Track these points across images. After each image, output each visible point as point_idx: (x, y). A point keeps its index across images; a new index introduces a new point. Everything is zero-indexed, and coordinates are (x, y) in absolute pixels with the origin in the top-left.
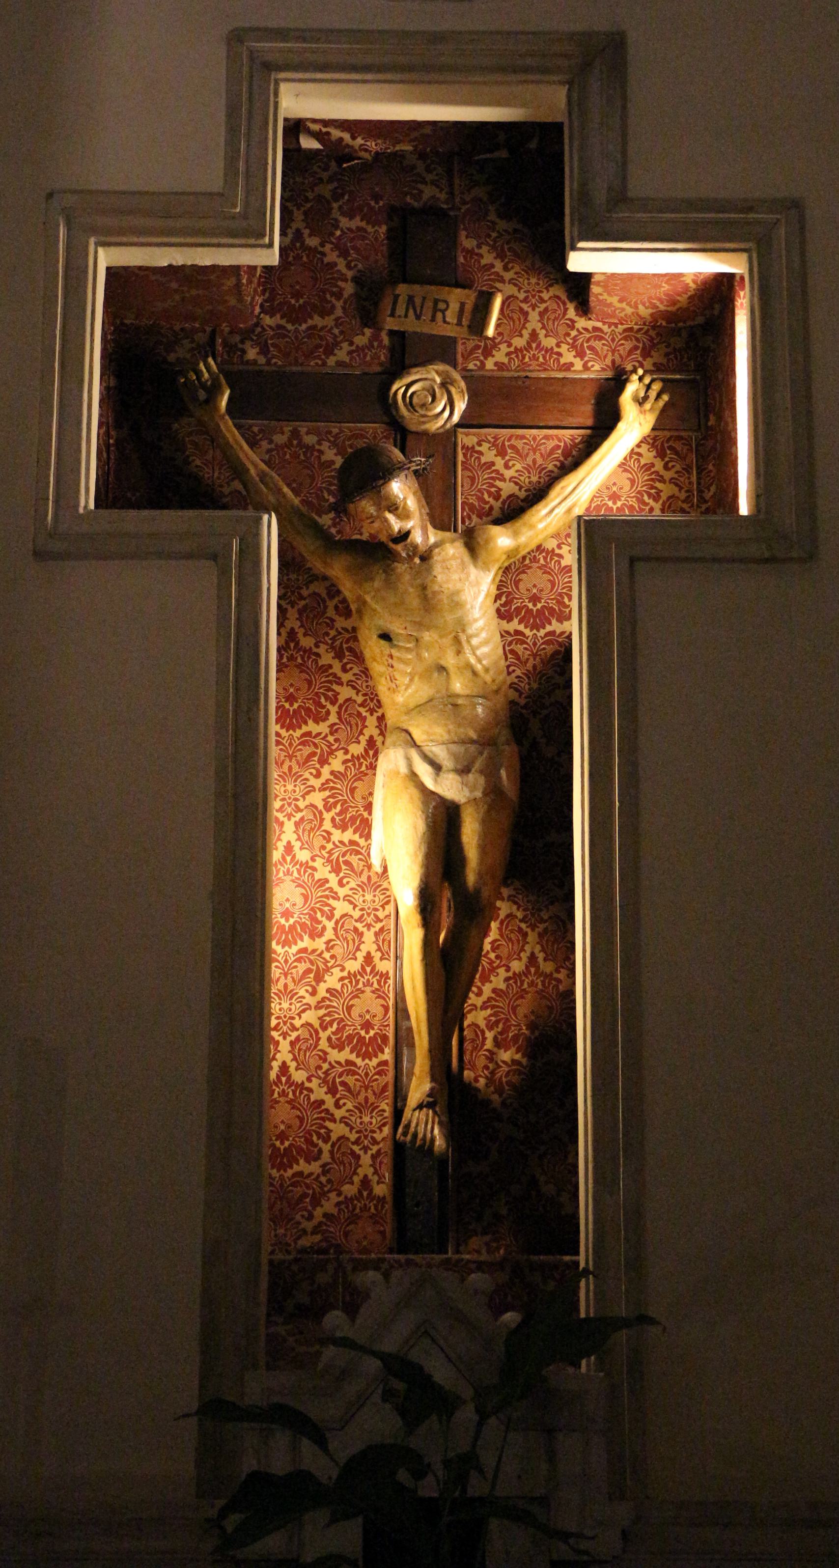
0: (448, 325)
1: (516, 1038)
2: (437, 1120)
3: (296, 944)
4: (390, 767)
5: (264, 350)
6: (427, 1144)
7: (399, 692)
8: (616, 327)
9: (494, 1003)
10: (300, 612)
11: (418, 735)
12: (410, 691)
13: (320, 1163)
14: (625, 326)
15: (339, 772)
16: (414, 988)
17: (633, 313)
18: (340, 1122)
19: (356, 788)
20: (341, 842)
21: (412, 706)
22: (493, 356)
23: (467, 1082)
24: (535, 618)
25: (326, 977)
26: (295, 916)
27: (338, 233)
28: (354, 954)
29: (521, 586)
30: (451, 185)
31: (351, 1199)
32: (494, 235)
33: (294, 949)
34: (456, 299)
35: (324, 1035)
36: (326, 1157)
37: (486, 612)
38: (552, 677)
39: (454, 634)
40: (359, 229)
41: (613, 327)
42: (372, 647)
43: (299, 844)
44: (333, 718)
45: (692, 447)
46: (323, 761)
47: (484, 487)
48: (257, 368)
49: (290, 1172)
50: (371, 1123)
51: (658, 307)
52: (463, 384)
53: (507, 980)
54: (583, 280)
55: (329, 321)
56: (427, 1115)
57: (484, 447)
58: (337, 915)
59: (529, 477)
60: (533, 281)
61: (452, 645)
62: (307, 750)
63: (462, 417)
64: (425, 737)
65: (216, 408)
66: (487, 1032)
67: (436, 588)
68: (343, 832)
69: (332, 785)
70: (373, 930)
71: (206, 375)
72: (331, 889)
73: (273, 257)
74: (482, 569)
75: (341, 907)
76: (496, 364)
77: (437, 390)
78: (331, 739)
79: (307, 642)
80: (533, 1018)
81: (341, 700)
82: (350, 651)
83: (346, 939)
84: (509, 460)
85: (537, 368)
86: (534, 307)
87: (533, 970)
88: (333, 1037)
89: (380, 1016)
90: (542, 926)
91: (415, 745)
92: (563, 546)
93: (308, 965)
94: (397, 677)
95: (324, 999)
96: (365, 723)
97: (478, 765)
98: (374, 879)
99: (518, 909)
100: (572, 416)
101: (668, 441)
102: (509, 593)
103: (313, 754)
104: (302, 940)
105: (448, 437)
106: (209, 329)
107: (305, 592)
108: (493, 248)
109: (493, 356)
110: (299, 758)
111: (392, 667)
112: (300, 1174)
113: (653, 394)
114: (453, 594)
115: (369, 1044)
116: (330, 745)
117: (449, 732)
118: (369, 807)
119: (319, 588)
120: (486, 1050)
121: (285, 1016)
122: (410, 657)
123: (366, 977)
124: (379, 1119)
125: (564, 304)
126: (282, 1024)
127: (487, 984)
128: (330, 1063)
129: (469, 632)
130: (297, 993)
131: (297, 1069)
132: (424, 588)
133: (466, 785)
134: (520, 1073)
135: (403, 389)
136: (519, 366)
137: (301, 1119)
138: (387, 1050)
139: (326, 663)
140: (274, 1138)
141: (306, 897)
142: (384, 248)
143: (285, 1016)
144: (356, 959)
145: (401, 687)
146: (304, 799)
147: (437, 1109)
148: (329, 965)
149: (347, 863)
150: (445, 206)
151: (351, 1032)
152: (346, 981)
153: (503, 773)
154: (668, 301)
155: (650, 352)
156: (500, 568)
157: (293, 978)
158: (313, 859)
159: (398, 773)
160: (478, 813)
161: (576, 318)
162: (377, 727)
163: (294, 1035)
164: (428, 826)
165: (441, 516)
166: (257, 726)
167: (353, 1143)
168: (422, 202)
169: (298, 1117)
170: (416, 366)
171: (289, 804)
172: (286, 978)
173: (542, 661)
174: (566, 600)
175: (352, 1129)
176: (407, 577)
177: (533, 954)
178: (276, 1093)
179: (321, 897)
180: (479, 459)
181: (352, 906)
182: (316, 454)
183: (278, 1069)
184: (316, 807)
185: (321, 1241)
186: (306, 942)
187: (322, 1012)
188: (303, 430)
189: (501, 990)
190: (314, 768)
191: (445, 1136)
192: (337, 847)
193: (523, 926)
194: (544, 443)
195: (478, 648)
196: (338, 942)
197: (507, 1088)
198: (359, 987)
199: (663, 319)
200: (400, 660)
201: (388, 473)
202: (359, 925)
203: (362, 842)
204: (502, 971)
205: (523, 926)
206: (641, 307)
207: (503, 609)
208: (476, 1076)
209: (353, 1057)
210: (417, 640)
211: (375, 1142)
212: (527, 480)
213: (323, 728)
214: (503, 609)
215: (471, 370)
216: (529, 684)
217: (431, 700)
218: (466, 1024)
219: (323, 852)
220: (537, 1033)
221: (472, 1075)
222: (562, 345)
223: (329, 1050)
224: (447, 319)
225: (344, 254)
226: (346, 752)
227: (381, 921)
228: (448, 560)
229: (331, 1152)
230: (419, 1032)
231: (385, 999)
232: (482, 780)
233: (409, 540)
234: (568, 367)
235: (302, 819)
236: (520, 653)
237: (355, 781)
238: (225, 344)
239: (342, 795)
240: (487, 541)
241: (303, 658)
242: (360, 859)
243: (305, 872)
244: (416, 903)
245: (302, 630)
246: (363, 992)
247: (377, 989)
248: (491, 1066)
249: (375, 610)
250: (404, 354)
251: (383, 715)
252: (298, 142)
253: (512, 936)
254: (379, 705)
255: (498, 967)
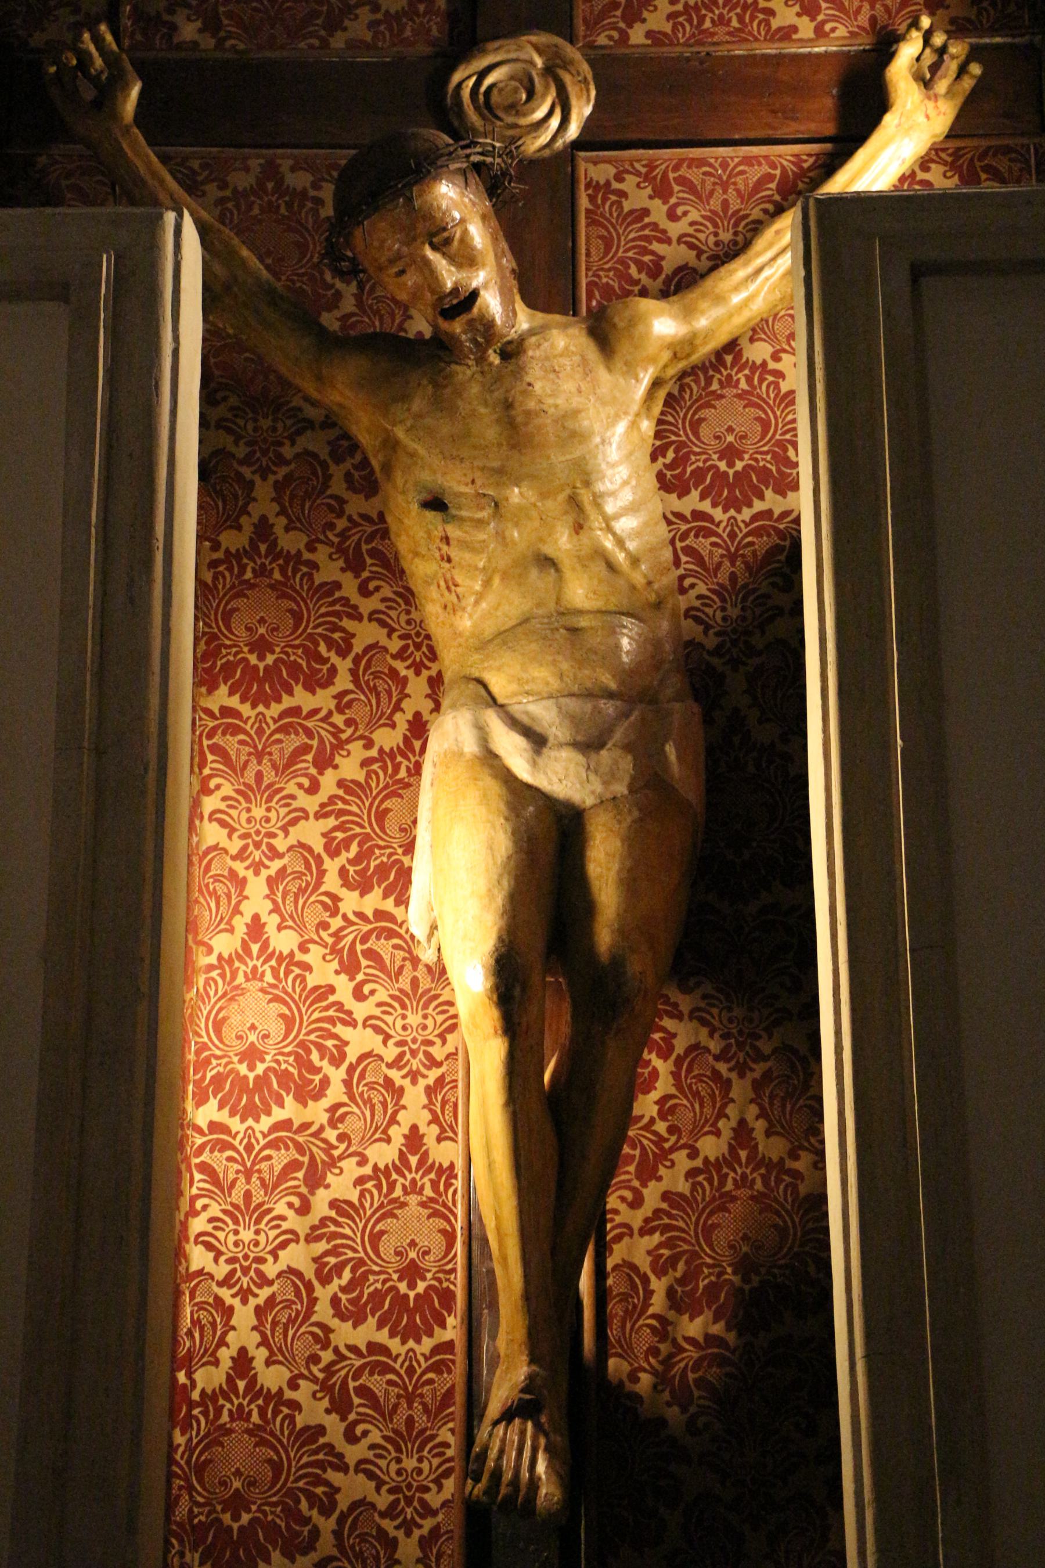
1: (712, 1290)
2: (542, 1441)
3: (269, 1113)
5: (212, 25)
11: (499, 685)
15: (353, 781)
16: (490, 1166)
19: (387, 811)
20: (360, 915)
21: (488, 633)
22: (644, 21)
23: (615, 1381)
24: (731, 488)
25: (330, 1178)
29: (704, 431)
33: (266, 1123)
35: (324, 1294)
37: (631, 454)
38: (767, 596)
39: (568, 491)
42: (413, 530)
43: (275, 919)
44: (343, 682)
46: (324, 762)
47: (630, 254)
50: (420, 1471)
52: (585, 68)
56: (523, 1433)
57: (629, 183)
59: (716, 234)
61: (566, 513)
63: (588, 126)
64: (514, 687)
65: (115, 116)
66: (653, 1278)
67: (532, 405)
68: (362, 895)
70: (422, 1083)
71: (99, 62)
72: (339, 1006)
75: (359, 1041)
76: (649, 34)
77: (537, 80)
78: (338, 719)
79: (291, 541)
81: (358, 648)
82: (376, 556)
87: (743, 1154)
88: (344, 1297)
89: (437, 1252)
90: (759, 1069)
91: (493, 701)
94: (459, 579)
95: (324, 1221)
96: (404, 675)
97: (618, 735)
99: (711, 1035)
100: (795, 119)
101: (983, 156)
102: (681, 445)
103: (305, 749)
104: (281, 1105)
105: (560, 165)
107: (288, 452)
109: (644, 21)
110: (275, 757)
111: (449, 560)
116: (337, 732)
118: (409, 848)
119: (315, 442)
120: (653, 1316)
124: (436, 1462)
126: (239, 1273)
128: (336, 1350)
129: (600, 487)
131: (268, 1363)
132: (508, 406)
134: (722, 1361)
135: (474, 79)
136: (693, 35)
137: (277, 1468)
138: (451, 1321)
141: (289, 1022)
144: (388, 1140)
145: (466, 599)
147: (543, 1419)
148: (336, 1153)
149: (370, 954)
152: (369, 1185)
153: (671, 751)
158: (303, 948)
159: (461, 754)
160: (620, 822)
162: (428, 696)
163: (265, 1293)
164: (516, 843)
165: (547, 278)
169: (270, 1461)
170: (496, 38)
171: (257, 845)
173: (748, 567)
176: (475, 389)
178: (225, 1412)
179: (318, 1020)
180: (619, 204)
182: (309, 205)
184: (310, 850)
186: (289, 1110)
187: (322, 1246)
188: (285, 165)
189: (681, 1195)
190: (306, 775)
191: (560, 1477)
193: (722, 1067)
195: (617, 517)
196: (355, 1109)
200: (465, 545)
201: (424, 168)
202: (395, 1075)
203: (398, 912)
204: (681, 1157)
205: (722, 1067)
207: (669, 473)
208: (631, 1369)
209: (382, 1337)
210: (496, 505)
211: (428, 1511)
212: (712, 240)
213: (323, 699)
214: (669, 473)
216: (723, 609)
217: (526, 620)
218: (610, 1263)
219: (324, 934)
220: (756, 1280)
221: (626, 1367)
223: (334, 1323)
226: (369, 744)
227: (439, 1065)
228: (555, 357)
229: (337, 1534)
230: (504, 1259)
231: (449, 1221)
232: (627, 764)
233: (475, 310)
234: (788, 33)
237: (386, 797)
240: (632, 323)
243: (287, 973)
244: (489, 985)
245: (283, 521)
249: (413, 455)
251: (440, 674)
255: (673, 1149)
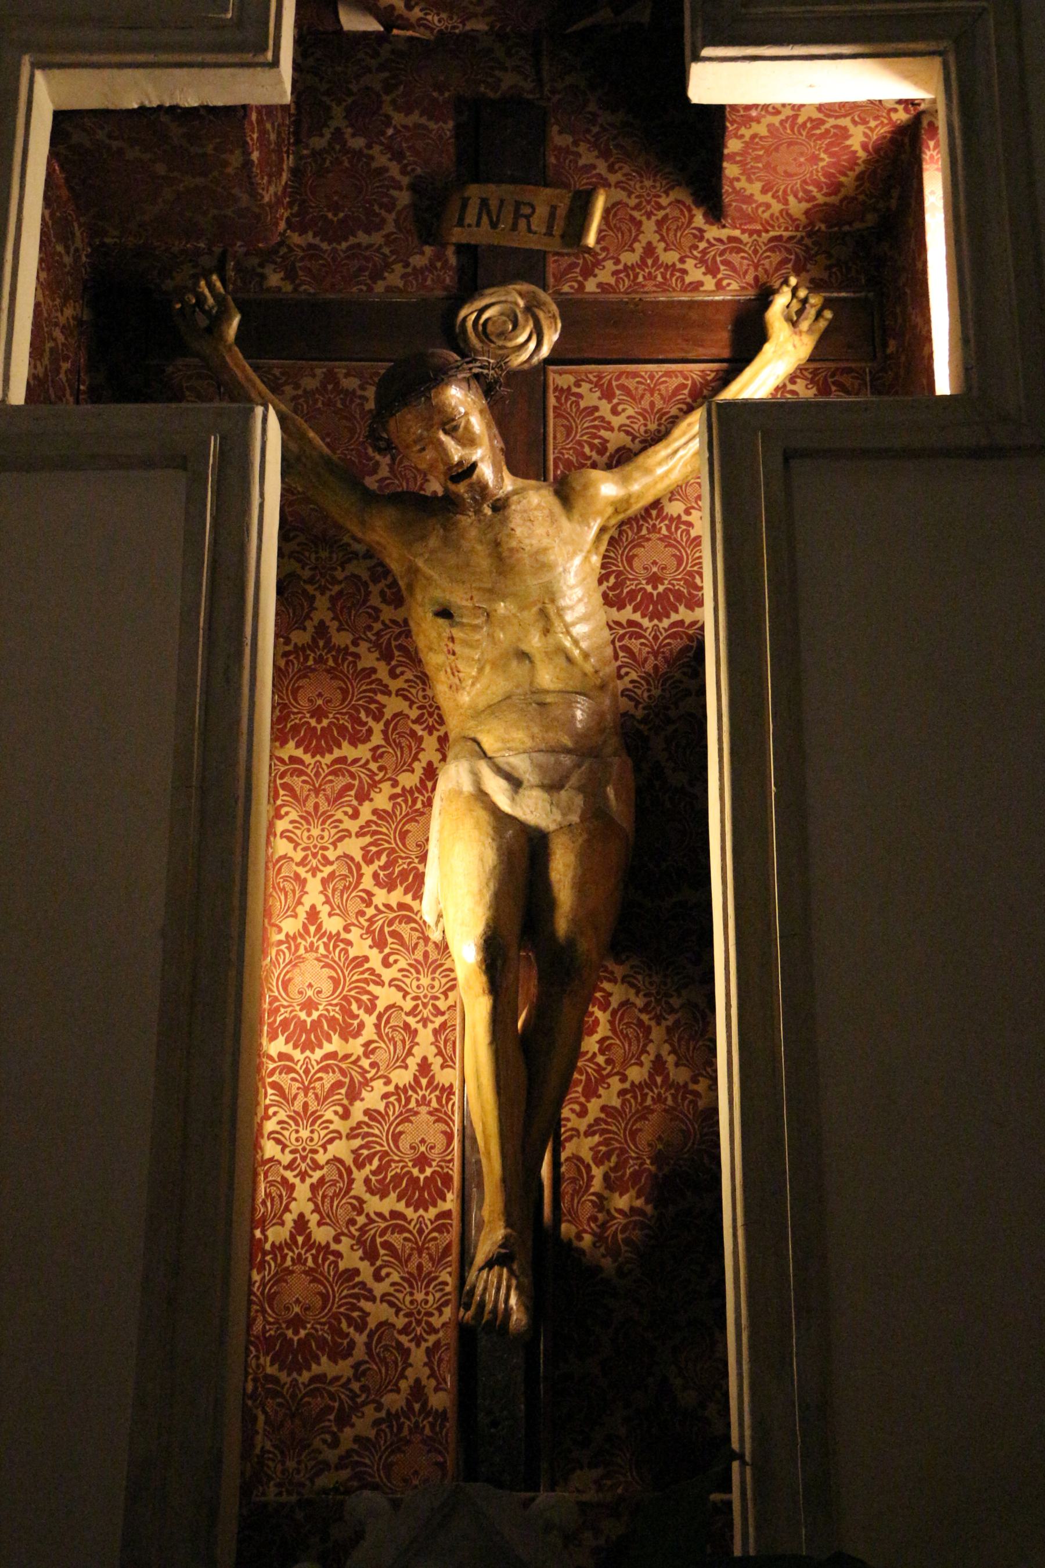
0: (532, 236)
1: (636, 1176)
2: (514, 1282)
3: (321, 1047)
4: (450, 786)
5: (290, 275)
6: (500, 1317)
7: (464, 688)
8: (760, 236)
9: (604, 1126)
10: (333, 600)
11: (489, 743)
12: (478, 686)
13: (350, 1361)
14: (772, 234)
16: (479, 1087)
17: (781, 211)
18: (382, 1301)
21: (481, 707)
24: (655, 604)
25: (364, 1094)
26: (321, 1007)
27: (390, 132)
28: (404, 1061)
29: (636, 563)
30: (538, 72)
31: (397, 1416)
32: (595, 130)
34: (544, 201)
35: (359, 1176)
36: (359, 1353)
39: (540, 606)
40: (417, 126)
41: (755, 237)
43: (326, 909)
44: (377, 739)
45: (864, 380)
46: (363, 797)
48: (281, 296)
49: (306, 1376)
51: (814, 198)
52: (554, 308)
53: (622, 1093)
54: (715, 117)
55: (377, 238)
58: (381, 1006)
59: (645, 425)
60: (648, 183)
62: (341, 782)
63: (554, 350)
64: (499, 745)
65: (221, 338)
67: (514, 544)
68: (389, 891)
69: (374, 828)
71: (211, 301)
73: (278, 84)
74: (579, 523)
75: (386, 996)
76: (600, 285)
77: (520, 315)
78: (374, 766)
80: (660, 1146)
82: (402, 651)
83: (392, 1039)
84: (618, 404)
85: (654, 289)
86: (649, 215)
90: (670, 1020)
91: (484, 755)
92: (692, 511)
93: (338, 1076)
94: (461, 667)
97: (574, 780)
98: (433, 955)
101: (833, 375)
104: (330, 1041)
105: (534, 378)
106: (217, 250)
108: (595, 145)
109: (595, 276)
111: (454, 654)
112: (320, 1378)
113: (811, 312)
114: (537, 553)
115: (311, 1031)
117: (533, 737)
118: (423, 858)
119: (360, 569)
120: (593, 1194)
121: (304, 1149)
122: (477, 637)
123: (421, 1093)
124: (438, 1295)
125: (690, 210)
127: (594, 1100)
129: (562, 603)
130: (321, 1116)
131: (320, 1224)
132: (497, 544)
133: (558, 806)
135: (475, 314)
136: (630, 286)
137: (325, 1298)
138: (450, 1196)
139: (368, 666)
140: (284, 1326)
141: (336, 982)
142: (452, 150)
143: (304, 1149)
144: (406, 1067)
145: (466, 680)
146: (336, 848)
147: (515, 1267)
149: (394, 934)
150: (531, 97)
151: (287, 1015)
153: (610, 791)
154: (828, 186)
155: (805, 265)
156: (603, 530)
157: (316, 1095)
159: (460, 792)
161: (706, 227)
162: (437, 750)
163: (317, 1175)
165: (525, 455)
166: (239, 688)
167: (400, 1332)
168: (500, 92)
169: (320, 1294)
172: (306, 1095)
174: (698, 580)
175: (398, 1310)
176: (473, 533)
177: (659, 1057)
178: (289, 1259)
181: (401, 994)
183: (292, 1224)
184: (352, 859)
185: (350, 1479)
186: (336, 1044)
187: (357, 1142)
188: (341, 372)
190: (350, 806)
191: (527, 1308)
192: (381, 912)
193: (645, 1017)
194: (665, 382)
195: (574, 624)
197: (624, 1248)
198: (410, 1106)
199: (822, 221)
201: (441, 376)
203: (414, 905)
205: (645, 1017)
206: (791, 199)
207: (611, 594)
208: (578, 1231)
212: (642, 429)
213: (362, 752)
214: (611, 594)
215: (567, 294)
217: (509, 697)
218: (563, 1156)
220: (666, 1169)
222: (687, 260)
223: (367, 1197)
224: (534, 228)
225: (398, 156)
227: (443, 1014)
229: (368, 1345)
231: (448, 1125)
232: (579, 800)
233: (474, 477)
234: (697, 286)
235: (332, 875)
236: (636, 651)
238: (238, 269)
239: (389, 843)
240: (586, 487)
241: (335, 660)
242: (413, 929)
243: (335, 947)
246: (416, 1113)
247: (436, 1110)
248: (601, 1216)
249: (429, 579)
250: (476, 273)
251: (446, 734)
252: (338, 21)
253: (630, 1031)
254: (441, 721)
